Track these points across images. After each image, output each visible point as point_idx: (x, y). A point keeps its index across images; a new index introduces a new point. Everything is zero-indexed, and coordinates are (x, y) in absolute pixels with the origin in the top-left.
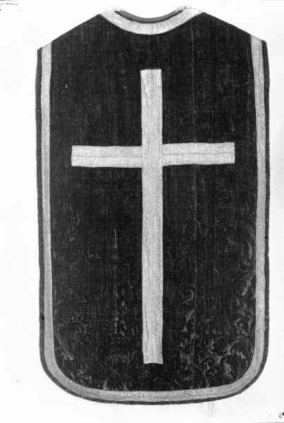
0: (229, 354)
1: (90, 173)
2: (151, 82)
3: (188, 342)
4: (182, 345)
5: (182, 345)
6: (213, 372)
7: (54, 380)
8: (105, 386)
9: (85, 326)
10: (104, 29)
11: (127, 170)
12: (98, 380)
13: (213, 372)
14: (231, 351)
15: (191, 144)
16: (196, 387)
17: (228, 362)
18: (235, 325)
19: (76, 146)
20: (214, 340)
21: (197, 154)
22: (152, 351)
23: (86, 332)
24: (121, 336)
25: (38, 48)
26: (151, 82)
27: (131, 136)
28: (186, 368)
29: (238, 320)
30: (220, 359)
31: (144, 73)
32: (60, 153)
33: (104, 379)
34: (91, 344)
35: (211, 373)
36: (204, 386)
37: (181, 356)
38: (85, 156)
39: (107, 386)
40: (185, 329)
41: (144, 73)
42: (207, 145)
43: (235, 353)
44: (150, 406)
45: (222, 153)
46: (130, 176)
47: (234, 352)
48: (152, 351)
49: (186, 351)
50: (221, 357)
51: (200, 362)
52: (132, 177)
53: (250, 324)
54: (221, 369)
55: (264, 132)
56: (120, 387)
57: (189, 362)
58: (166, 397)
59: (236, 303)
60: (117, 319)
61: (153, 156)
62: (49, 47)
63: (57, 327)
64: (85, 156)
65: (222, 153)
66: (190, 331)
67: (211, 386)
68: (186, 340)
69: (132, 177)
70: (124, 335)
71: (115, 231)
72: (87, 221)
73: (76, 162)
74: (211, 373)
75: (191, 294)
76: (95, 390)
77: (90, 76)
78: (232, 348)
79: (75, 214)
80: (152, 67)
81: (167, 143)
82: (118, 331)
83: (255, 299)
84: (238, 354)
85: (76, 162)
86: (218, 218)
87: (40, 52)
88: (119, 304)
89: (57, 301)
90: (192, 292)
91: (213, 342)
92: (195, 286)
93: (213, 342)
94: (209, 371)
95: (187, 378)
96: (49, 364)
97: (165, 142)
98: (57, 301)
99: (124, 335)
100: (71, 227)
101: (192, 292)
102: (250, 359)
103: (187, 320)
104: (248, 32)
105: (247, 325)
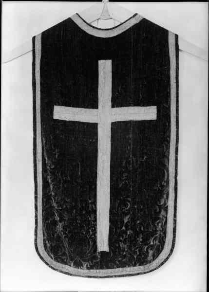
0: (152, 243)
2: (105, 67)
4: (121, 239)
5: (121, 239)
20: (142, 235)
22: (103, 245)
26: (105, 67)
27: (93, 103)
28: (125, 253)
30: (146, 248)
31: (101, 63)
37: (121, 246)
40: (124, 228)
41: (101, 63)
45: (149, 113)
47: (154, 242)
48: (103, 245)
50: (147, 246)
59: (156, 210)
61: (105, 116)
64: (62, 113)
65: (149, 113)
67: (140, 265)
72: (63, 158)
75: (128, 205)
77: (66, 61)
80: (106, 58)
86: (146, 159)
90: (129, 204)
101: (129, 204)
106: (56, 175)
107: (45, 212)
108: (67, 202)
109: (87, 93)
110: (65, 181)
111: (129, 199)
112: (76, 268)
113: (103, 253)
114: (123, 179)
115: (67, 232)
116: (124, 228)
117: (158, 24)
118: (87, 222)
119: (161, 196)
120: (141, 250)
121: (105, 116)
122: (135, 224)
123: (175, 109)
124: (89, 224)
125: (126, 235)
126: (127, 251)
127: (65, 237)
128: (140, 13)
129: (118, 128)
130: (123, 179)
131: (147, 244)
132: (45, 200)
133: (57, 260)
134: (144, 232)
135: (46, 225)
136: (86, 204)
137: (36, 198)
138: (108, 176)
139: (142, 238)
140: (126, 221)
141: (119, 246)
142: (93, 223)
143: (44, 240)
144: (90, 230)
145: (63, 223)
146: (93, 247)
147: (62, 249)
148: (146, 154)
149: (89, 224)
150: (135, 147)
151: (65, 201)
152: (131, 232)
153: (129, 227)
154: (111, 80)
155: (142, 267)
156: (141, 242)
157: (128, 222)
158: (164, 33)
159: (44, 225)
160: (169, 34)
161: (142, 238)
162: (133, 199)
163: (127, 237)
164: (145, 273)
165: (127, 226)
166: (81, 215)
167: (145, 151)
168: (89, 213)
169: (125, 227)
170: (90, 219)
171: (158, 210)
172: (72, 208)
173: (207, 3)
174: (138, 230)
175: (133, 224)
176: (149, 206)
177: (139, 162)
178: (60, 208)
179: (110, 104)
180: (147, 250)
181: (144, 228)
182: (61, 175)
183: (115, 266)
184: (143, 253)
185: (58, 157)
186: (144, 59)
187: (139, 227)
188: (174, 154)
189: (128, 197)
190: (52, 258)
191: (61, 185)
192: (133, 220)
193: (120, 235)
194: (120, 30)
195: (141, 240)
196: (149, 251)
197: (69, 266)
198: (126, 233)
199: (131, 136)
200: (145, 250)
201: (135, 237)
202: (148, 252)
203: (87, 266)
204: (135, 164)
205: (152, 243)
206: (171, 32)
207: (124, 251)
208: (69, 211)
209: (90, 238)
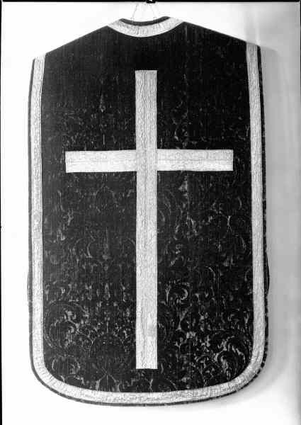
0: (225, 349)
2: (146, 83)
4: (177, 344)
5: (177, 344)
6: (210, 370)
9: (77, 325)
12: (90, 381)
13: (210, 370)
19: (71, 152)
23: (78, 330)
24: (112, 336)
25: (33, 58)
26: (146, 83)
30: (216, 356)
31: (139, 75)
33: (97, 379)
35: (208, 372)
38: (80, 162)
40: (180, 328)
41: (139, 75)
43: (231, 349)
44: (265, 115)
45: (219, 161)
46: (172, 284)
50: (218, 354)
51: (197, 361)
53: (246, 321)
56: (113, 389)
58: (158, 399)
64: (80, 162)
65: (219, 161)
70: (116, 336)
72: (83, 222)
73: (70, 169)
74: (208, 372)
75: (184, 293)
77: (86, 89)
78: (228, 343)
79: (66, 214)
83: (252, 295)
84: (233, 349)
85: (70, 169)
86: (213, 228)
88: (111, 304)
90: (186, 291)
91: (208, 340)
94: (207, 369)
95: (184, 379)
99: (116, 336)
100: (62, 226)
101: (186, 291)
102: (248, 355)
103: (181, 319)
105: (244, 321)
106: (69, 251)
107: (48, 310)
110: (83, 260)
111: (188, 284)
114: (177, 253)
120: (210, 360)
121: (147, 160)
125: (184, 340)
127: (86, 348)
130: (177, 253)
132: (47, 292)
133: (67, 373)
134: (213, 332)
136: (118, 293)
142: (129, 321)
148: (212, 213)
151: (84, 291)
156: (208, 348)
162: (194, 284)
165: (184, 326)
166: (112, 309)
168: (124, 307)
172: (95, 300)
173: (298, 5)
174: (202, 329)
175: (194, 322)
176: (218, 292)
177: (200, 227)
178: (77, 301)
180: (219, 359)
181: (211, 328)
182: (77, 251)
185: (71, 223)
187: (203, 325)
188: (261, 212)
191: (76, 266)
193: (175, 339)
194: (140, 398)
195: (208, 345)
201: (199, 341)
203: (121, 385)
206: (249, 44)
207: (181, 364)
208: (92, 305)
209: (125, 344)
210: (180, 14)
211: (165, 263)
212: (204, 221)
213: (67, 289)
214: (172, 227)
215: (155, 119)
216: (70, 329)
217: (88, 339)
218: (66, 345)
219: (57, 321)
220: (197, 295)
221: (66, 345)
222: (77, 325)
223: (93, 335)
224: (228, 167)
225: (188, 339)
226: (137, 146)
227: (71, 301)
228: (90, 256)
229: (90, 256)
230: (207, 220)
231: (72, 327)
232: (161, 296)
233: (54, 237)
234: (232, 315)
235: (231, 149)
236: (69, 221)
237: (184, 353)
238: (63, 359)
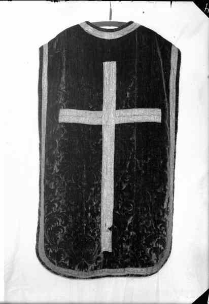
0: (154, 246)
1: (68, 126)
2: (110, 69)
3: (129, 237)
5: (124, 239)
7: (43, 264)
8: (76, 268)
10: (79, 50)
11: (93, 126)
13: (144, 258)
14: (156, 245)
15: (133, 109)
16: (132, 266)
17: (154, 252)
18: (159, 227)
20: (145, 237)
21: (136, 115)
22: (106, 242)
25: (133, 20)
26: (110, 69)
27: (97, 105)
28: (127, 254)
29: (161, 224)
30: (149, 250)
31: (106, 64)
32: (53, 112)
34: (68, 244)
36: (137, 266)
37: (124, 246)
39: (78, 267)
40: (127, 229)
41: (106, 64)
42: (144, 109)
45: (152, 115)
47: (157, 245)
48: (106, 242)
49: (128, 242)
52: (97, 130)
54: (149, 258)
55: (175, 104)
57: (128, 250)
59: (159, 213)
60: (85, 225)
61: (110, 117)
62: (47, 45)
63: (46, 231)
64: (69, 116)
66: (130, 230)
67: (142, 267)
68: (127, 236)
69: (97, 130)
71: (84, 166)
72: (68, 159)
76: (70, 271)
77: (74, 62)
80: (110, 59)
81: (119, 109)
82: (86, 233)
86: (148, 158)
87: (41, 49)
89: (47, 214)
91: (145, 239)
92: (133, 201)
93: (145, 239)
96: (40, 254)
97: (117, 108)
98: (47, 214)
104: (171, 42)
108: (72, 205)
109: (92, 96)
112: (80, 271)
113: (105, 253)
115: (72, 235)
116: (127, 229)
117: (153, 30)
118: (92, 224)
119: (163, 200)
122: (138, 226)
123: (174, 114)
124: (95, 227)
126: (130, 252)
128: (135, 21)
129: (122, 130)
131: (149, 246)
132: (46, 207)
135: (48, 232)
137: (40, 192)
138: (76, 112)
139: (145, 241)
140: (129, 222)
141: (122, 246)
143: (46, 247)
144: (96, 232)
145: (68, 226)
146: (98, 249)
147: (64, 255)
148: (150, 156)
149: (95, 227)
150: (138, 149)
152: (134, 233)
153: (132, 228)
154: (115, 82)
155: (144, 269)
157: (131, 223)
158: (166, 46)
159: (45, 232)
160: (173, 49)
161: (145, 241)
163: (130, 238)
164: (147, 276)
165: (130, 227)
167: (149, 153)
169: (128, 228)
170: (95, 221)
171: (161, 214)
172: (77, 211)
174: (140, 232)
177: (143, 165)
179: (114, 105)
182: (65, 179)
183: (117, 266)
184: (146, 255)
186: (147, 64)
189: (131, 198)
190: (55, 264)
192: (136, 221)
196: (152, 253)
197: (72, 270)
198: (129, 235)
199: (135, 138)
200: (148, 252)
202: (151, 255)
204: (139, 166)
205: (154, 246)
210: (125, 13)
211: (119, 187)
212: (145, 161)
213: (59, 204)
214: (125, 163)
215: (129, 122)
216: (60, 231)
217: (71, 237)
218: (58, 242)
219: (53, 226)
220: (139, 208)
221: (58, 242)
222: (65, 228)
223: (75, 235)
224: (113, 64)
225: (131, 236)
226: (103, 109)
227: (61, 212)
228: (74, 182)
229: (74, 182)
230: (147, 161)
231: (62, 230)
232: (116, 209)
233: (52, 171)
234: (161, 224)
235: (160, 108)
236: (61, 159)
237: (128, 244)
238: (56, 251)
